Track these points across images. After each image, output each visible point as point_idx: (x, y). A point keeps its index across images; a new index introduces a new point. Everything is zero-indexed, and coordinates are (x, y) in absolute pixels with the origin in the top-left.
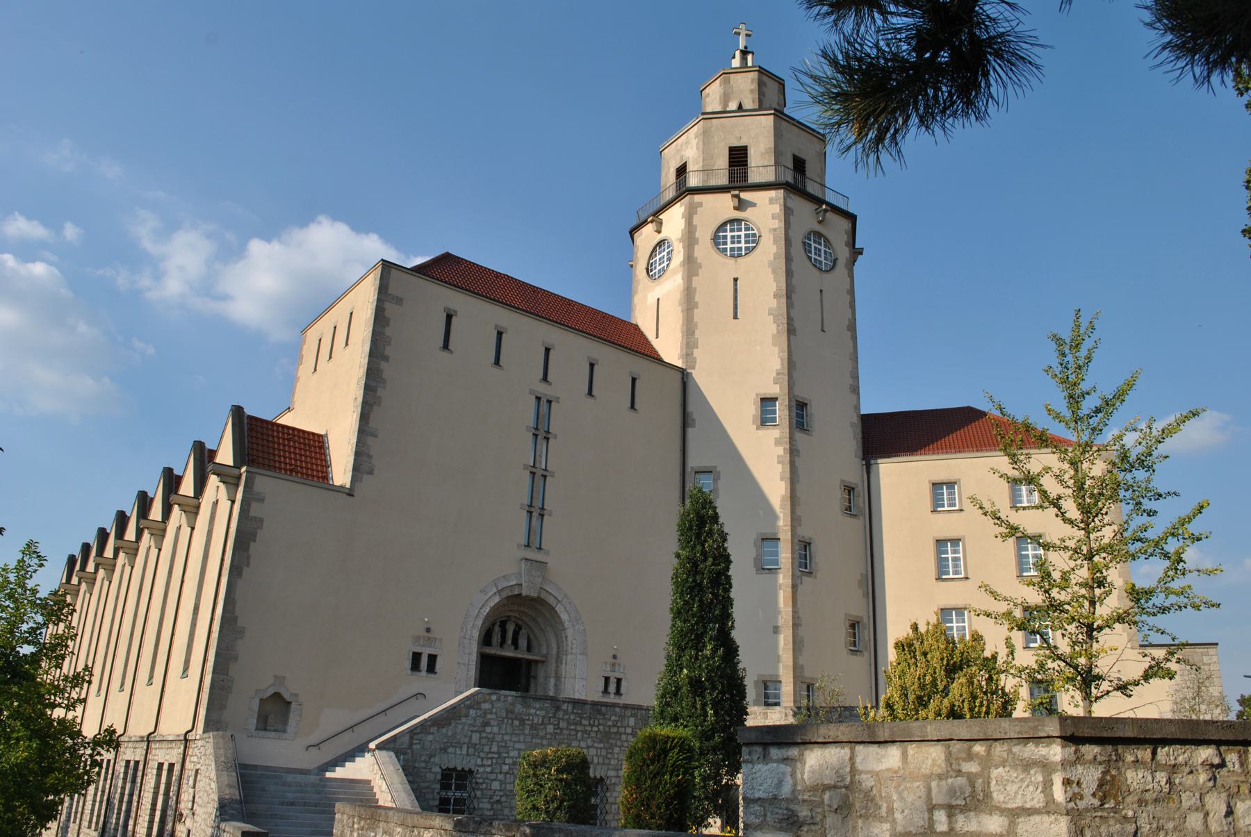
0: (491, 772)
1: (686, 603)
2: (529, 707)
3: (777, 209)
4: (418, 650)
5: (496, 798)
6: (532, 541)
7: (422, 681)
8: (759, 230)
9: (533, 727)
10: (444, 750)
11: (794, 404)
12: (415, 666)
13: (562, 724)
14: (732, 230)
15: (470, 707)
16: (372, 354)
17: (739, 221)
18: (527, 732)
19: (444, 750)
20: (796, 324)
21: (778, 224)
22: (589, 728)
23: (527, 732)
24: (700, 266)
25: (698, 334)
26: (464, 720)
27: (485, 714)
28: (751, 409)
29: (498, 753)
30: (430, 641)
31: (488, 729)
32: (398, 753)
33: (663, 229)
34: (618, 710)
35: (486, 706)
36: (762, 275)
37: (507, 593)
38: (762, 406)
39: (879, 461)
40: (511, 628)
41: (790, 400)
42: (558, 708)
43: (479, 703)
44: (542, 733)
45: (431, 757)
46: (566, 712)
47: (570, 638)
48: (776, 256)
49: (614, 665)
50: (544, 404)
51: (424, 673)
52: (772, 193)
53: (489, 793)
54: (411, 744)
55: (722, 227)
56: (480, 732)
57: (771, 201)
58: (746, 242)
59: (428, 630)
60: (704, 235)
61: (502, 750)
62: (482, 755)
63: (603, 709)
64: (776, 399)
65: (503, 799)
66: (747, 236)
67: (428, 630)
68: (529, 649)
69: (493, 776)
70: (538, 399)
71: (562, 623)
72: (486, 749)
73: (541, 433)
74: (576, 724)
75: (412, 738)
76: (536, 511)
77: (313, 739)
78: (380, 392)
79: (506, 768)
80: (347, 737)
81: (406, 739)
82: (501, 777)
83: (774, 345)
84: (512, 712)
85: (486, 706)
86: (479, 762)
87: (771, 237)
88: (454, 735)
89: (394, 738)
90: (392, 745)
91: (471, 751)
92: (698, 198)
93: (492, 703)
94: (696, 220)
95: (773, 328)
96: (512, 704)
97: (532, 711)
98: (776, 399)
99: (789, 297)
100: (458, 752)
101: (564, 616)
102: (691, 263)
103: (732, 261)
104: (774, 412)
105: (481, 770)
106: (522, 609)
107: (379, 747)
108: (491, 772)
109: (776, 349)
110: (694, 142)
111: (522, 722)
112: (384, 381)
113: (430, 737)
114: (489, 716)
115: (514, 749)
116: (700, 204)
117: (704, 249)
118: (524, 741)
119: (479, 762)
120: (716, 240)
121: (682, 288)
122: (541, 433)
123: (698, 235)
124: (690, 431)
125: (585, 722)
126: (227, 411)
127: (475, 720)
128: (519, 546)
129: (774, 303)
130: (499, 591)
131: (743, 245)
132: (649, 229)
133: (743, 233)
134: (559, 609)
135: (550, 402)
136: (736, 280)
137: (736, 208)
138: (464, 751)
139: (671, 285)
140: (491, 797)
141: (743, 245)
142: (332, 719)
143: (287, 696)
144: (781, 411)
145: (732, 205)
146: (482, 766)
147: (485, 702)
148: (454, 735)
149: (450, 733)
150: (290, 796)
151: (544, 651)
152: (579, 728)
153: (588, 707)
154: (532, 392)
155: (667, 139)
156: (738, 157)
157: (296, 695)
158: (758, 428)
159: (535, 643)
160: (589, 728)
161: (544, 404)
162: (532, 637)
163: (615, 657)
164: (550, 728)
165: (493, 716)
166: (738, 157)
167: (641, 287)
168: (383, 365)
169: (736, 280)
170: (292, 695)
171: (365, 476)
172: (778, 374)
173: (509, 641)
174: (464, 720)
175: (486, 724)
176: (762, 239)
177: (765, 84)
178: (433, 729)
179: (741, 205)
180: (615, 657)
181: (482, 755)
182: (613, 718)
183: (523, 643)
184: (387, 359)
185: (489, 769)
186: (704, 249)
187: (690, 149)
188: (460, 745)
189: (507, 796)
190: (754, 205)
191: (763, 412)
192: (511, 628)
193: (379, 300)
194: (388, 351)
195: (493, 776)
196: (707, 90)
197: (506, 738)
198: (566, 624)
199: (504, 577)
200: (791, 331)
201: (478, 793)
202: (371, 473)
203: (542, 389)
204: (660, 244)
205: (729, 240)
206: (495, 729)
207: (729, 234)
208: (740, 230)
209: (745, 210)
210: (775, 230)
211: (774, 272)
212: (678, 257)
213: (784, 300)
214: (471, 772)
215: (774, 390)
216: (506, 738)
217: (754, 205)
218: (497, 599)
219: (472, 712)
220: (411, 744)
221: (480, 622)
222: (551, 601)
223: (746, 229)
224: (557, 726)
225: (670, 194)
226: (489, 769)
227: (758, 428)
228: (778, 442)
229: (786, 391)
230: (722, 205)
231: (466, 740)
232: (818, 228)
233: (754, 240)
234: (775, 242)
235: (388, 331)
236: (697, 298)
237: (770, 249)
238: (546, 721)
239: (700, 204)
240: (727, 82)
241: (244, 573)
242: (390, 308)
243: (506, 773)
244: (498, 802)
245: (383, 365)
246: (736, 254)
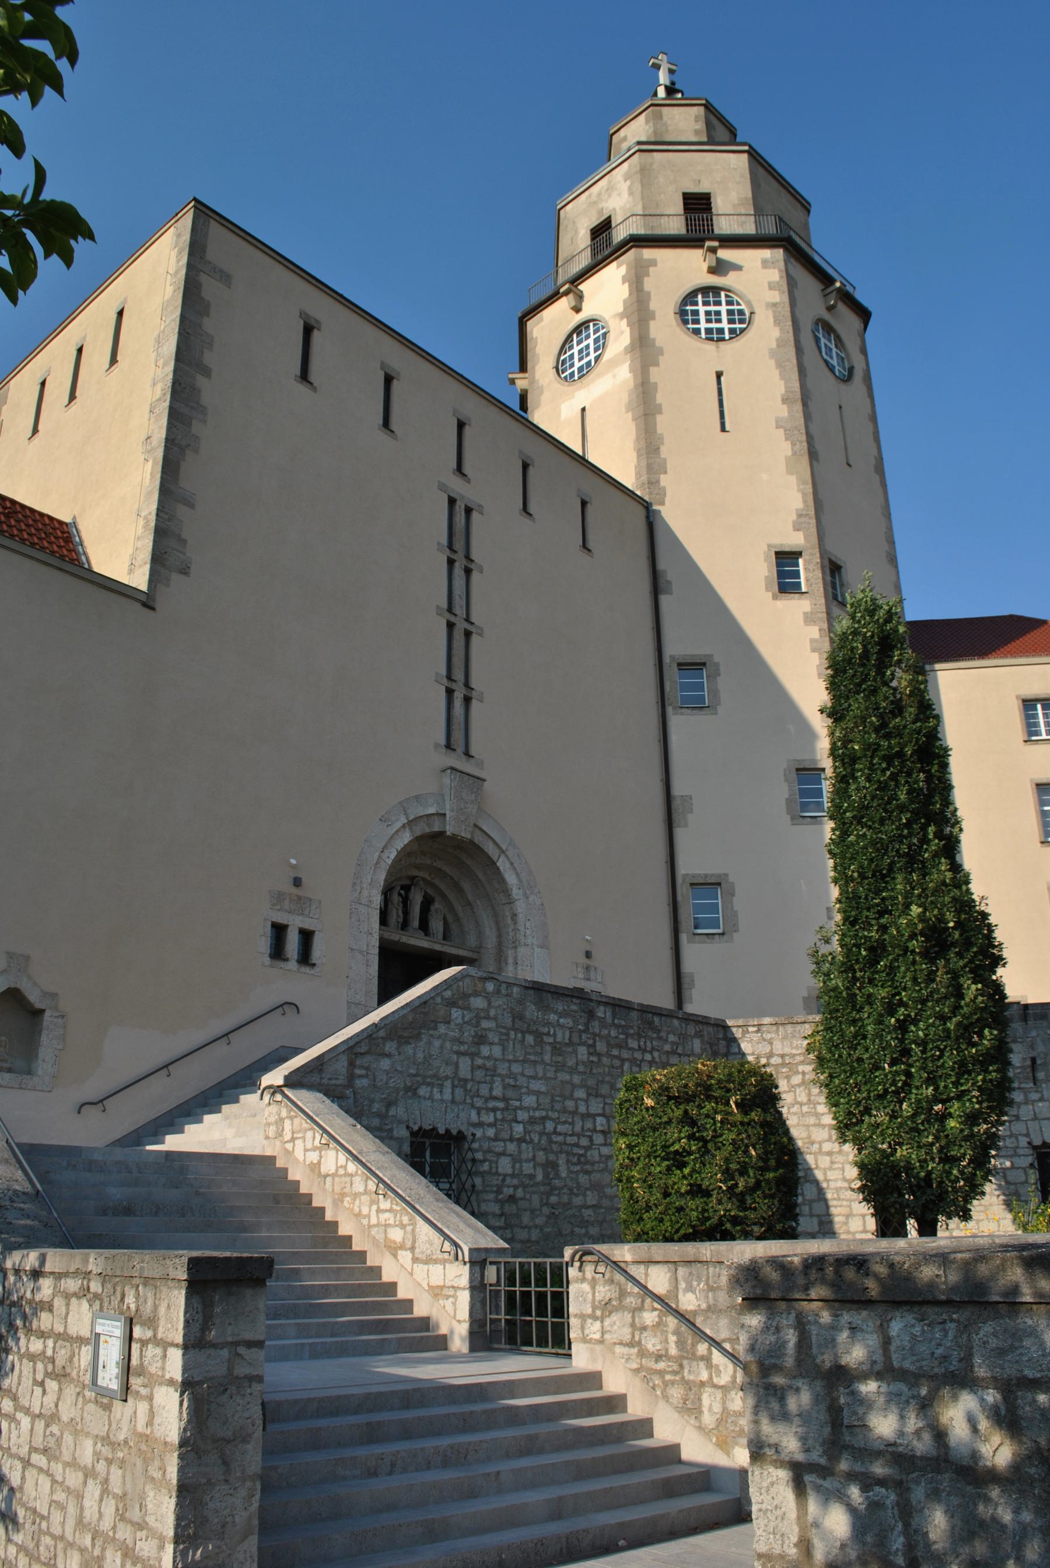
0: (496, 1139)
1: (883, 787)
2: (547, 1009)
3: (775, 275)
4: (281, 918)
5: (508, 1191)
6: (457, 737)
7: (288, 982)
8: (749, 304)
9: (556, 1049)
10: (412, 1091)
11: (827, 563)
12: (278, 952)
13: (601, 1047)
14: (705, 303)
15: (451, 1003)
16: (181, 356)
17: (716, 290)
18: (547, 1058)
19: (412, 1091)
20: (818, 446)
21: (779, 297)
22: (638, 1055)
23: (547, 1058)
24: (660, 352)
25: (664, 451)
26: (442, 1029)
27: (478, 1018)
28: (764, 569)
29: (505, 1099)
30: (302, 904)
31: (485, 1050)
32: (333, 1094)
33: (585, 306)
34: (676, 1022)
35: (478, 1003)
36: (761, 368)
37: (421, 829)
38: (778, 565)
39: (937, 666)
40: (417, 899)
41: (822, 557)
42: (591, 1015)
43: (466, 996)
44: (571, 1062)
45: (389, 1104)
46: (602, 1020)
47: (521, 917)
48: (780, 343)
49: (588, 968)
50: (460, 516)
51: (292, 965)
52: (766, 253)
53: (496, 1181)
54: (351, 1077)
55: (690, 298)
56: (473, 1055)
57: (765, 264)
58: (731, 321)
59: (297, 882)
60: (664, 307)
61: (510, 1093)
62: (479, 1102)
63: (656, 1019)
64: (799, 554)
65: (520, 1193)
66: (730, 313)
67: (297, 882)
68: (446, 937)
69: (499, 1147)
70: (452, 501)
71: (506, 891)
72: (484, 1090)
73: (459, 557)
74: (620, 1047)
75: (352, 1064)
76: (459, 690)
77: (92, 1089)
78: (196, 427)
79: (519, 1129)
80: (157, 1085)
81: (341, 1066)
82: (511, 1147)
83: (789, 472)
84: (521, 1018)
85: (478, 1003)
86: (474, 1117)
87: (770, 313)
88: (428, 1058)
89: (319, 1063)
90: (315, 1078)
91: (459, 1092)
92: (648, 253)
93: (488, 997)
94: (648, 284)
95: (785, 448)
96: (521, 1002)
97: (553, 1017)
98: (799, 554)
99: (805, 405)
100: (437, 1096)
101: (511, 879)
102: (644, 350)
103: (710, 347)
104: (797, 575)
105: (479, 1133)
106: (438, 864)
107: (294, 1081)
108: (496, 1139)
109: (793, 479)
110: (624, 186)
111: (539, 1036)
112: (204, 411)
113: (385, 1064)
114: (485, 1024)
115: (530, 1092)
116: (653, 263)
117: (665, 326)
118: (545, 1078)
119: (474, 1117)
120: (685, 315)
121: (631, 384)
122: (459, 557)
123: (653, 305)
124: (663, 599)
125: (633, 1044)
126: (36, 109)
127: (461, 1027)
128: (437, 746)
129: (783, 411)
130: (410, 823)
131: (725, 325)
132: (563, 304)
133: (723, 309)
134: (502, 864)
135: (468, 511)
136: (719, 375)
137: (712, 271)
138: (447, 1096)
139: (612, 381)
140: (499, 1191)
141: (725, 325)
142: (129, 1049)
143: (34, 997)
144: (809, 572)
145: (705, 267)
146: (480, 1125)
147: (476, 994)
148: (428, 1058)
149: (420, 1056)
150: (116, 1193)
151: (472, 941)
152: (625, 1054)
153: (634, 1015)
154: (442, 487)
155: (570, 188)
156: (697, 205)
157: (54, 996)
158: (775, 598)
159: (454, 928)
160: (638, 1055)
161: (460, 516)
162: (450, 919)
163: (588, 955)
164: (582, 1050)
165: (491, 1024)
166: (697, 205)
167: (545, 397)
168: (201, 381)
169: (719, 375)
170: (46, 994)
171: (175, 577)
172: (800, 516)
173: (416, 923)
174: (442, 1029)
175: (481, 1039)
176: (757, 318)
177: (714, 128)
178: (390, 1047)
179: (719, 268)
180: (588, 955)
181: (479, 1102)
182: (672, 1038)
183: (436, 925)
184: (207, 372)
185: (491, 1132)
186: (665, 326)
187: (615, 195)
188: (437, 1081)
189: (525, 1187)
190: (738, 268)
191: (781, 575)
192: (417, 899)
193: (190, 266)
194: (209, 358)
195: (499, 1147)
196: (622, 133)
197: (516, 1068)
198: (516, 893)
199: (417, 798)
200: (813, 455)
201: (478, 1181)
202: (185, 571)
203: (457, 485)
204: (580, 329)
205: (702, 317)
206: (497, 1051)
207: (702, 309)
208: (719, 303)
209: (725, 275)
210: (775, 305)
211: (779, 365)
212: (620, 338)
213: (798, 407)
214: (461, 1137)
215: (795, 540)
216: (516, 1068)
217: (738, 268)
218: (406, 838)
219: (456, 1014)
220: (351, 1077)
221: (382, 877)
222: (490, 849)
223: (729, 303)
224: (592, 1050)
225: (584, 261)
226: (491, 1132)
227: (775, 598)
228: (809, 619)
229: (815, 540)
230: (689, 267)
231: (449, 1071)
232: (827, 316)
233: (741, 320)
234: (777, 322)
235: (208, 324)
236: (660, 398)
237: (768, 331)
238: (576, 1039)
239: (653, 263)
240: (659, 117)
241: (206, 399)
242: (210, 288)
243: (521, 1140)
244: (512, 1199)
245: (201, 381)
246: (715, 337)
